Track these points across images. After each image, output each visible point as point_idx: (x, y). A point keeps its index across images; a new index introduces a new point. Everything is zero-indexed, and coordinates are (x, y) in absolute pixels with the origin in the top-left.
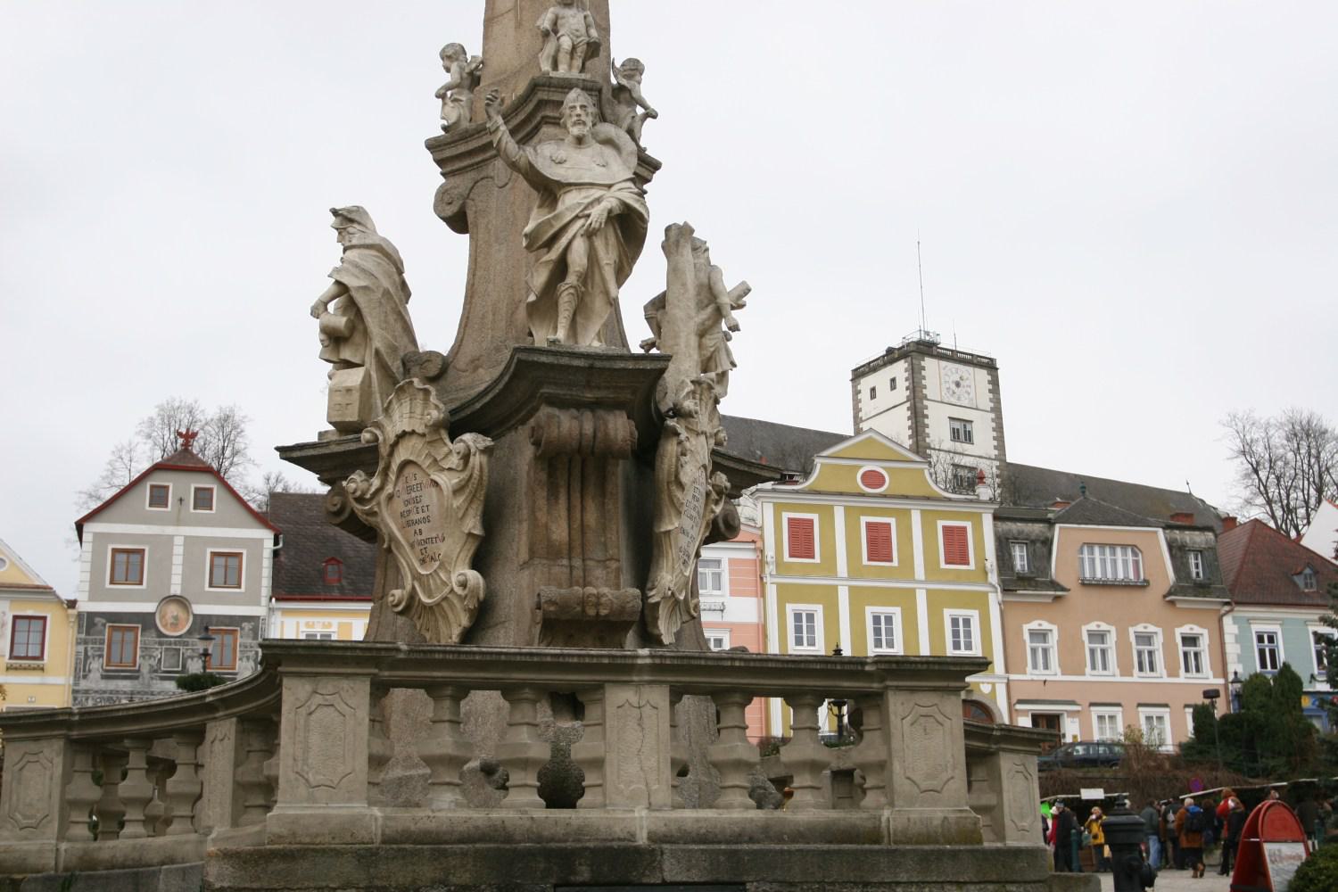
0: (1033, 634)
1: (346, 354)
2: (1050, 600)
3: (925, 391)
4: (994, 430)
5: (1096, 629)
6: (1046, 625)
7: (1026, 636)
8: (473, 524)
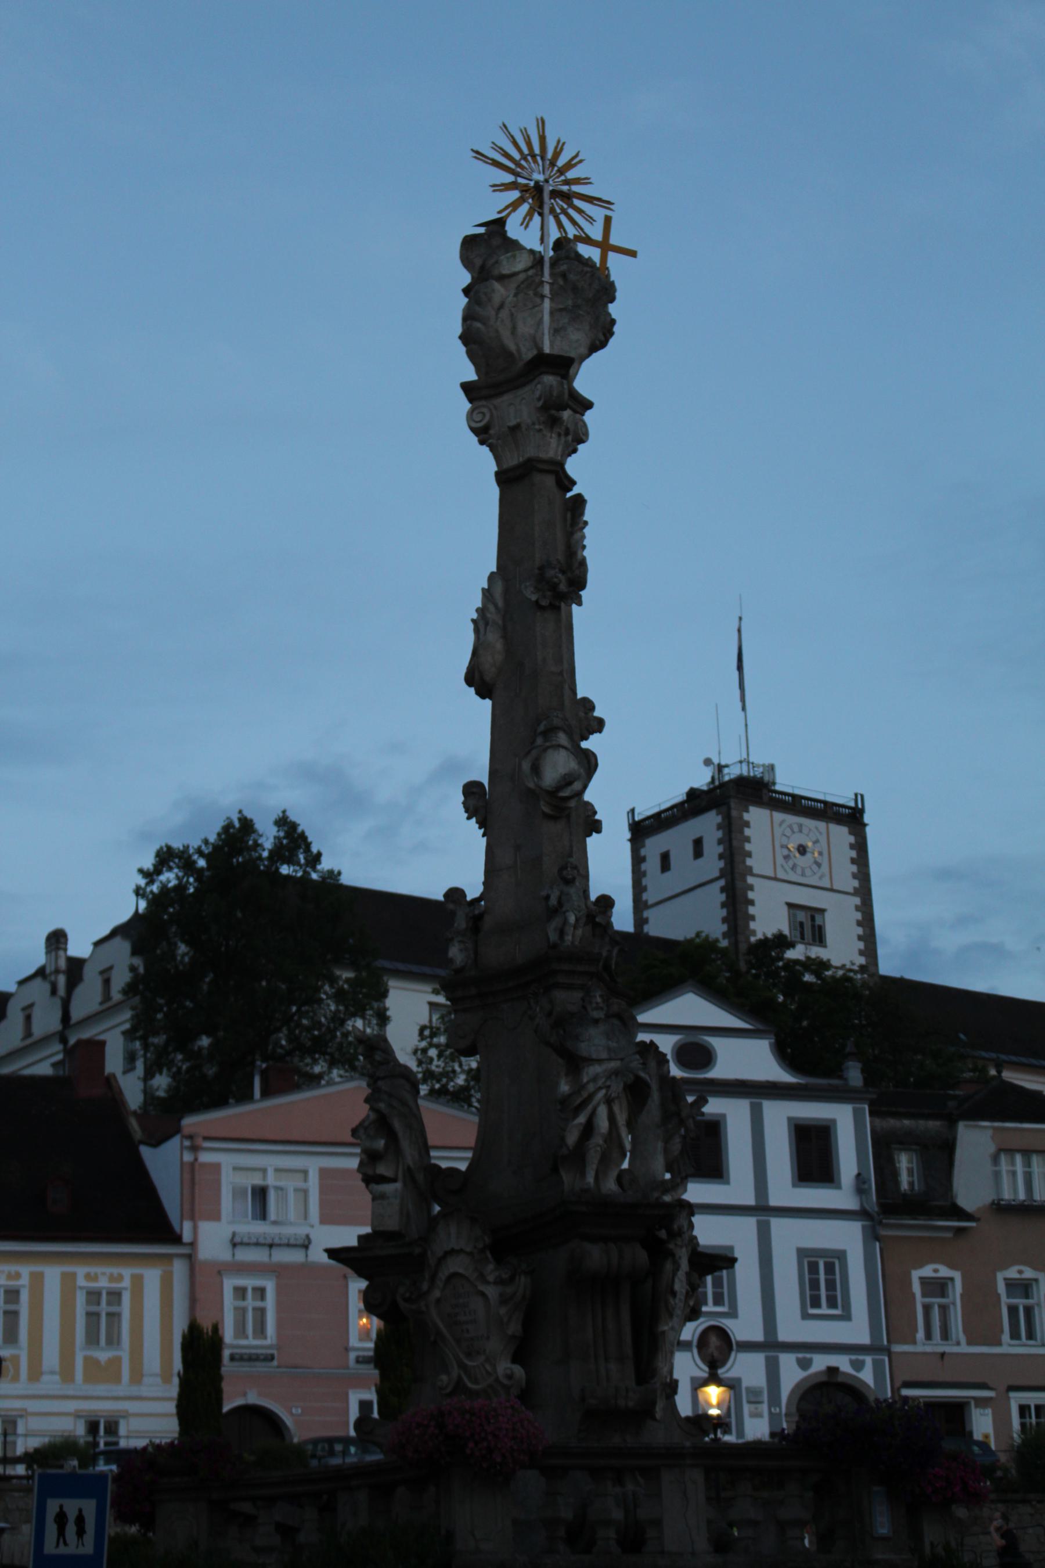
1: (382, 1169)
3: (749, 862)
4: (859, 923)
5: (1017, 1276)
6: (944, 1272)
8: (514, 1328)
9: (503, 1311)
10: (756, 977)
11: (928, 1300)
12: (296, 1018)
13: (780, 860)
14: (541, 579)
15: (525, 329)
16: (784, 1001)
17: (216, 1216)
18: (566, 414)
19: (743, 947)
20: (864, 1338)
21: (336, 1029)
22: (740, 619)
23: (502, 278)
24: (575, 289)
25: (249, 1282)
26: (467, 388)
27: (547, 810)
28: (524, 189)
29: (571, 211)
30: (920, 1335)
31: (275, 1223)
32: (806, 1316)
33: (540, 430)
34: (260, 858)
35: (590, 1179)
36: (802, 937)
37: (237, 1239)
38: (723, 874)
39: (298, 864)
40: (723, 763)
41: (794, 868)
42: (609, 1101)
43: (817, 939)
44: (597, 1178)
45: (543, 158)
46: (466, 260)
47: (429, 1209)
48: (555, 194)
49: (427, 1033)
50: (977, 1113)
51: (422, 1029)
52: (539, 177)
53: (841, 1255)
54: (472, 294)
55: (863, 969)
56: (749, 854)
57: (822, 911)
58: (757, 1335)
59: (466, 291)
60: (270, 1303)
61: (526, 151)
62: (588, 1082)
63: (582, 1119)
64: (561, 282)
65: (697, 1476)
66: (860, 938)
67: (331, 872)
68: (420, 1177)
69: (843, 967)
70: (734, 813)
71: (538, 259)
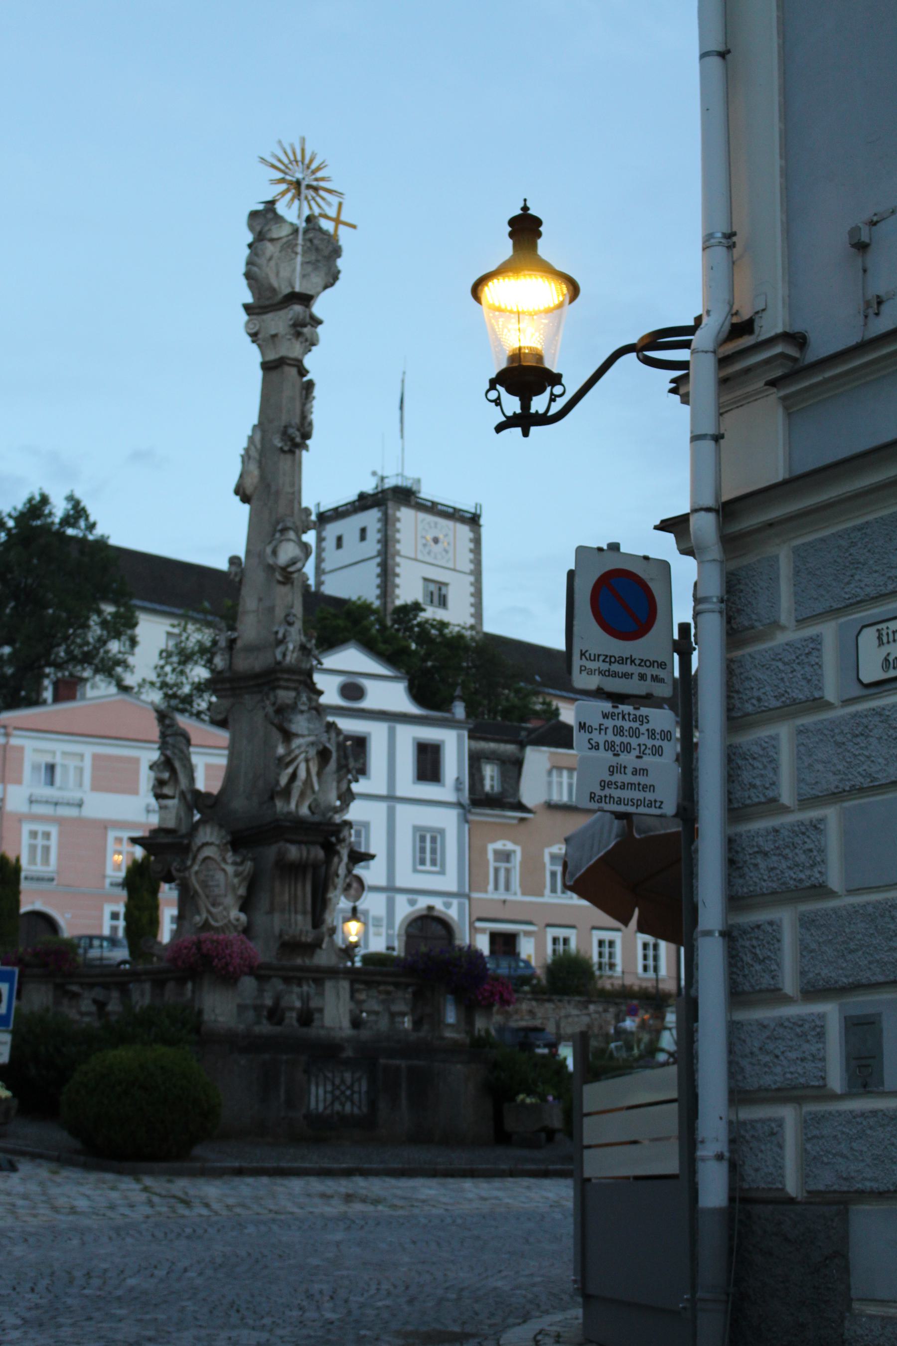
0: (497, 853)
2: (515, 822)
4: (472, 595)
6: (509, 846)
7: (491, 856)
8: (242, 891)
9: (236, 881)
10: (398, 630)
11: (499, 864)
12: (72, 637)
13: (420, 547)
14: (285, 434)
15: (284, 273)
16: (416, 648)
17: (19, 781)
18: (306, 330)
19: (390, 608)
20: (453, 887)
21: (99, 648)
22: (404, 373)
23: (272, 240)
24: (317, 250)
25: (40, 828)
26: (247, 308)
27: (280, 578)
28: (290, 183)
29: (318, 199)
30: (491, 887)
31: (60, 788)
32: (415, 870)
33: (290, 339)
34: (53, 523)
35: (293, 805)
36: (432, 601)
37: (34, 798)
38: (379, 554)
39: (79, 528)
40: (385, 474)
41: (429, 553)
42: (307, 761)
43: (442, 603)
44: (297, 806)
45: (303, 163)
46: (251, 227)
47: (192, 816)
48: (309, 187)
49: (164, 654)
50: (541, 740)
51: (161, 652)
52: (299, 176)
53: (442, 832)
54: (253, 247)
55: (472, 627)
56: (398, 541)
57: (446, 584)
58: (382, 882)
59: (250, 246)
60: (53, 843)
61: (292, 158)
62: (296, 748)
63: (290, 770)
64: (308, 244)
65: (345, 985)
66: (472, 605)
67: (102, 536)
68: (189, 797)
69: (459, 625)
70: (390, 511)
71: (296, 231)
